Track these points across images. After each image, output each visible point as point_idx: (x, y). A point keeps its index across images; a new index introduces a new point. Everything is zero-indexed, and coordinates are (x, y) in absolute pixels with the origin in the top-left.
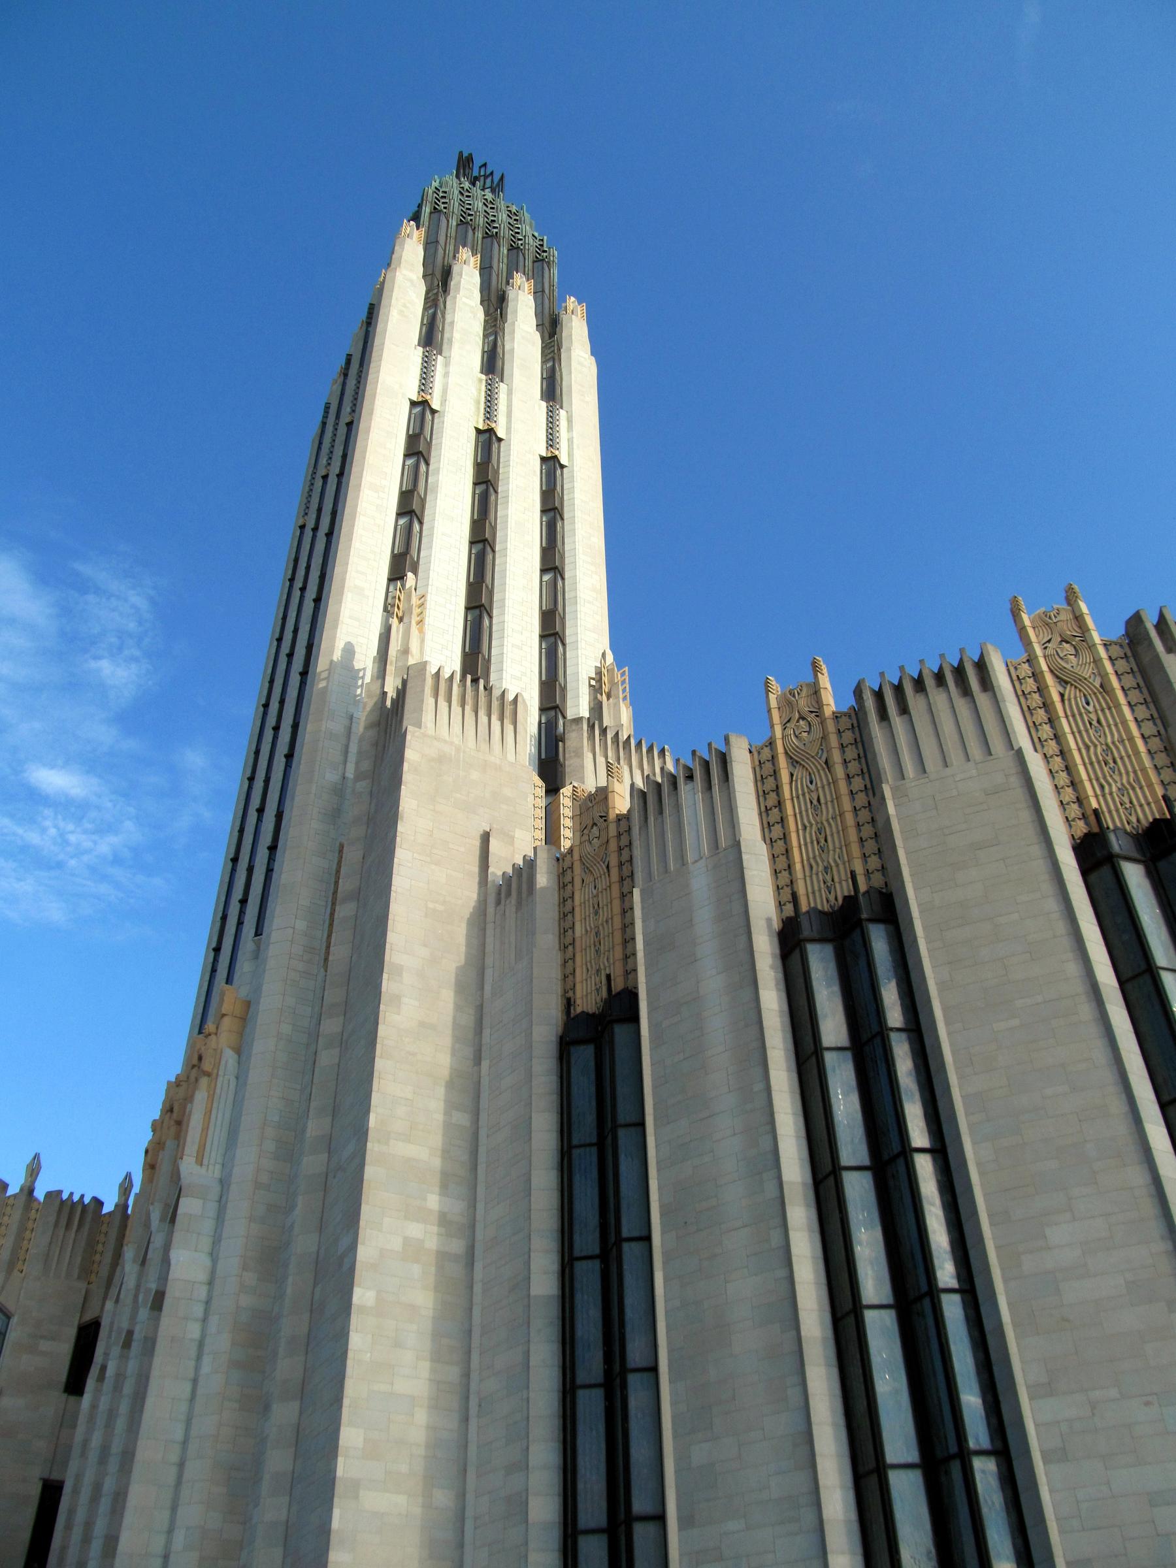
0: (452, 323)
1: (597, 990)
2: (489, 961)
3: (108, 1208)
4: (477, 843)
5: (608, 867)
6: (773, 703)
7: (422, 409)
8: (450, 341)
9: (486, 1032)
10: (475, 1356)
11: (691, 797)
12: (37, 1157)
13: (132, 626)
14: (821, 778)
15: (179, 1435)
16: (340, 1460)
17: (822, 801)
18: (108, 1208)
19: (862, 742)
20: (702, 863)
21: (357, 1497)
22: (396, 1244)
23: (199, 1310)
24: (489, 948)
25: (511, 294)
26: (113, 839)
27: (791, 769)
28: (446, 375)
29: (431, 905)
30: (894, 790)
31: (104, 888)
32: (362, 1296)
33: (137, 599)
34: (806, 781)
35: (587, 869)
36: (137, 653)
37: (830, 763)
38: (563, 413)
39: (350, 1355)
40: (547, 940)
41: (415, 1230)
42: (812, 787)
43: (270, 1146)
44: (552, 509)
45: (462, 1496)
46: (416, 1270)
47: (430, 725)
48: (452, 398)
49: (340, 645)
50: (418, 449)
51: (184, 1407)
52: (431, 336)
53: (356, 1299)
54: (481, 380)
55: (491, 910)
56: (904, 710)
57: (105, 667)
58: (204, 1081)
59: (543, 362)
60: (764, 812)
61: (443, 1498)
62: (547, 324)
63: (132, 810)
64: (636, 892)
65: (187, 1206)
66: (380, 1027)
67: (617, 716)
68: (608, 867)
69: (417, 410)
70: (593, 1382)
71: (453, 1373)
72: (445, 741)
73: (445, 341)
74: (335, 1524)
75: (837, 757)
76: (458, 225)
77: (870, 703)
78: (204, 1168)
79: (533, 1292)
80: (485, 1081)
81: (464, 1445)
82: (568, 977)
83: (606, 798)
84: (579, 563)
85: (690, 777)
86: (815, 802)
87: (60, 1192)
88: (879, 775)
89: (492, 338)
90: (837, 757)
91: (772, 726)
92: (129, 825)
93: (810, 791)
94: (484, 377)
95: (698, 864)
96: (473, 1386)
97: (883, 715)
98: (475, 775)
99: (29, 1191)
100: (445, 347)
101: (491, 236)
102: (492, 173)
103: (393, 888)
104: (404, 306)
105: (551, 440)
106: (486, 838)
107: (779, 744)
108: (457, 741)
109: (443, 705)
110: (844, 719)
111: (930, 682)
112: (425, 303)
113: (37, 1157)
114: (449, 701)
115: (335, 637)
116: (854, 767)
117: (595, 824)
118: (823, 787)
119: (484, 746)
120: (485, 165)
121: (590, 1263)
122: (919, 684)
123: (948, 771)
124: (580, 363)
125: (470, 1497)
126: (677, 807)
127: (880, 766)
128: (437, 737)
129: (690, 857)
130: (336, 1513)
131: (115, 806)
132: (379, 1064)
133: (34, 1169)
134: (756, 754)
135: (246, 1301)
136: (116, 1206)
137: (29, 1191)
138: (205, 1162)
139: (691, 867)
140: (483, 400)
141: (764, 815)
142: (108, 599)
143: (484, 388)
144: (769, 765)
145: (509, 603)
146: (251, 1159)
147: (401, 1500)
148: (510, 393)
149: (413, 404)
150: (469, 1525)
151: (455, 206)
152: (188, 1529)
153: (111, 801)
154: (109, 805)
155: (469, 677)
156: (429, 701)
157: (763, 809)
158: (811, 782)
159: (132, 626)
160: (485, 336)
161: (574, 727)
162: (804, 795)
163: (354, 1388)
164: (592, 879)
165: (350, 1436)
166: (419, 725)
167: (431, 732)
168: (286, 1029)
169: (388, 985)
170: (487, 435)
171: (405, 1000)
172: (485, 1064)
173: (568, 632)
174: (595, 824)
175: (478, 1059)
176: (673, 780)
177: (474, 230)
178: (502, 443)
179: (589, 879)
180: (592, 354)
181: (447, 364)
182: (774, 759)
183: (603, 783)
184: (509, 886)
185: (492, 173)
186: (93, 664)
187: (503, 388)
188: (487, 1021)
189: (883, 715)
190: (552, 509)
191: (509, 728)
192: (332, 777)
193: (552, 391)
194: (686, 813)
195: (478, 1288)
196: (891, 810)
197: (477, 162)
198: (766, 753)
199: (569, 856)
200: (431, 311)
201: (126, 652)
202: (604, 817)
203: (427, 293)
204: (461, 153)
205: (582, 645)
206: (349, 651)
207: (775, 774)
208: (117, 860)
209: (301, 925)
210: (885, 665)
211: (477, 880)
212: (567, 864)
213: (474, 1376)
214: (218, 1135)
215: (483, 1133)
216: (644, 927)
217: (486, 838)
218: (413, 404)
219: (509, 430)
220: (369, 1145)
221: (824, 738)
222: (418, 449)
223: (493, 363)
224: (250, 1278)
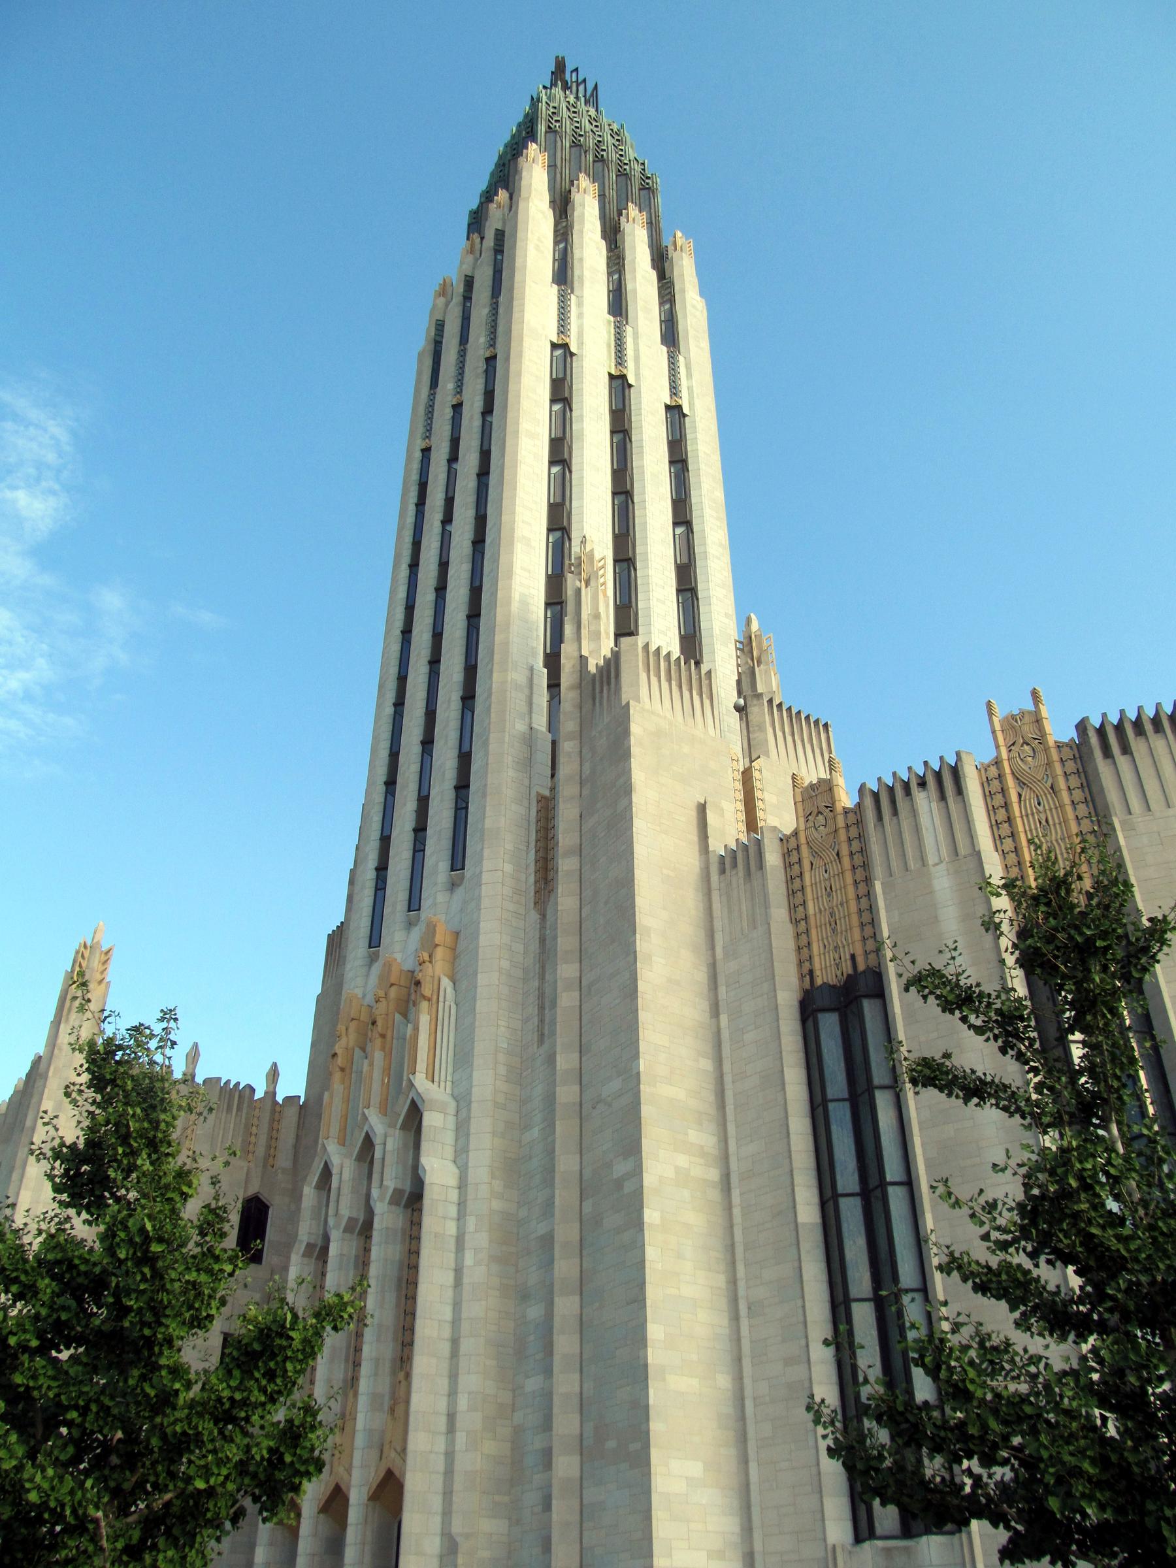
0: (581, 260)
1: (837, 965)
2: (718, 924)
3: (259, 1094)
4: (693, 814)
5: (838, 854)
6: (998, 727)
7: (562, 352)
8: (581, 278)
9: (722, 990)
10: (740, 1268)
11: (924, 801)
12: (275, 1066)
13: (51, 457)
14: (1048, 802)
15: (448, 1315)
16: (650, 1350)
17: (1051, 822)
18: (259, 1094)
19: (1085, 772)
20: (942, 867)
21: (664, 1380)
22: (670, 1173)
23: (453, 1211)
24: (717, 912)
25: (576, 197)
26: (24, 675)
27: (1020, 790)
28: (580, 316)
29: (665, 871)
30: (1122, 823)
31: (13, 725)
32: (651, 1215)
33: (56, 429)
34: (1034, 802)
35: (814, 853)
36: (57, 487)
37: (1056, 789)
38: (681, 358)
39: (647, 1264)
40: (779, 914)
41: (682, 1160)
42: (1041, 808)
43: (502, 1070)
44: (679, 459)
45: (739, 1378)
46: (686, 1193)
47: (647, 700)
48: (644, 372)
49: (516, 596)
50: (561, 392)
51: (449, 1293)
52: (564, 273)
53: (647, 1218)
54: (609, 322)
55: (715, 877)
56: (1126, 750)
57: (21, 498)
58: (424, 1005)
59: (661, 304)
60: (995, 825)
61: (724, 1381)
62: (558, 202)
63: (44, 646)
64: (878, 886)
65: (430, 1119)
66: (639, 982)
67: (768, 683)
68: (838, 854)
69: (559, 352)
70: (864, 1296)
71: (721, 1280)
72: (659, 715)
73: (576, 278)
74: (651, 1402)
75: (845, 851)
76: (571, 147)
77: (1094, 740)
78: (436, 1084)
79: (800, 1220)
80: (725, 1034)
81: (737, 1339)
82: (803, 949)
83: (831, 789)
84: (707, 517)
85: (922, 784)
86: (1044, 822)
87: (219, 1079)
88: (1107, 807)
89: (616, 277)
90: (1062, 783)
91: (997, 747)
92: (41, 662)
93: (1039, 812)
94: (612, 319)
95: (938, 867)
96: (741, 1292)
97: (1107, 753)
98: (686, 749)
99: (271, 1094)
100: (576, 285)
101: (600, 160)
102: (584, 81)
103: (635, 855)
104: (539, 240)
105: (674, 389)
106: (702, 809)
107: (1006, 764)
108: (669, 714)
109: (654, 679)
110: (1066, 750)
111: (1148, 727)
112: (555, 236)
113: (275, 1066)
114: (680, 687)
115: (510, 588)
116: (1078, 795)
117: (819, 813)
118: (1051, 810)
119: (690, 720)
120: (576, 70)
121: (851, 1199)
122: (1138, 725)
123: (1171, 812)
124: (694, 307)
125: (747, 1382)
126: (914, 813)
127: (1108, 799)
128: (651, 710)
129: (931, 859)
130: (651, 1392)
131: (26, 641)
132: (642, 1015)
133: (273, 1074)
134: (983, 771)
135: (496, 1205)
136: (266, 1093)
137: (271, 1094)
138: (436, 1079)
139: (933, 869)
140: (613, 343)
141: (995, 828)
142: (27, 427)
143: (613, 331)
144: (996, 783)
145: (651, 556)
146: (487, 1081)
147: (695, 1382)
148: (636, 336)
149: (554, 346)
150: (749, 1404)
151: (568, 127)
152: (469, 1393)
153: (23, 636)
154: (21, 640)
155: (692, 662)
156: (643, 676)
157: (994, 822)
158: (1039, 804)
159: (51, 457)
160: (610, 274)
161: (755, 702)
162: (1033, 814)
163: (654, 1293)
164: (822, 863)
165: (654, 1331)
166: (638, 700)
167: (647, 706)
168: (505, 964)
169: (641, 946)
170: (620, 381)
171: (654, 958)
172: (724, 1019)
173: (700, 587)
174: (819, 813)
175: (715, 1011)
176: (906, 786)
177: (561, 138)
178: (632, 390)
179: (818, 862)
180: (701, 295)
181: (580, 304)
182: (1000, 777)
183: (823, 775)
184: (735, 858)
185: (584, 81)
186: (9, 494)
187: (629, 330)
188: (721, 979)
189: (1107, 753)
190: (679, 459)
191: (707, 702)
192: (521, 727)
193: (670, 336)
194: (924, 820)
195: (736, 1211)
196: (1122, 841)
197: (569, 67)
198: (993, 771)
199: (793, 839)
200: (562, 246)
201: (44, 484)
202: (831, 808)
203: (556, 225)
204: (557, 57)
205: (713, 600)
206: (525, 603)
207: (1003, 791)
208: (28, 697)
209: (508, 868)
210: (1107, 704)
211: (697, 848)
212: (793, 843)
213: (741, 1285)
214: (445, 1056)
215: (728, 1079)
216: (888, 918)
217: (702, 809)
218: (554, 346)
219: (638, 375)
220: (642, 1087)
221: (1049, 764)
222: (561, 392)
223: (618, 304)
224: (498, 1185)
